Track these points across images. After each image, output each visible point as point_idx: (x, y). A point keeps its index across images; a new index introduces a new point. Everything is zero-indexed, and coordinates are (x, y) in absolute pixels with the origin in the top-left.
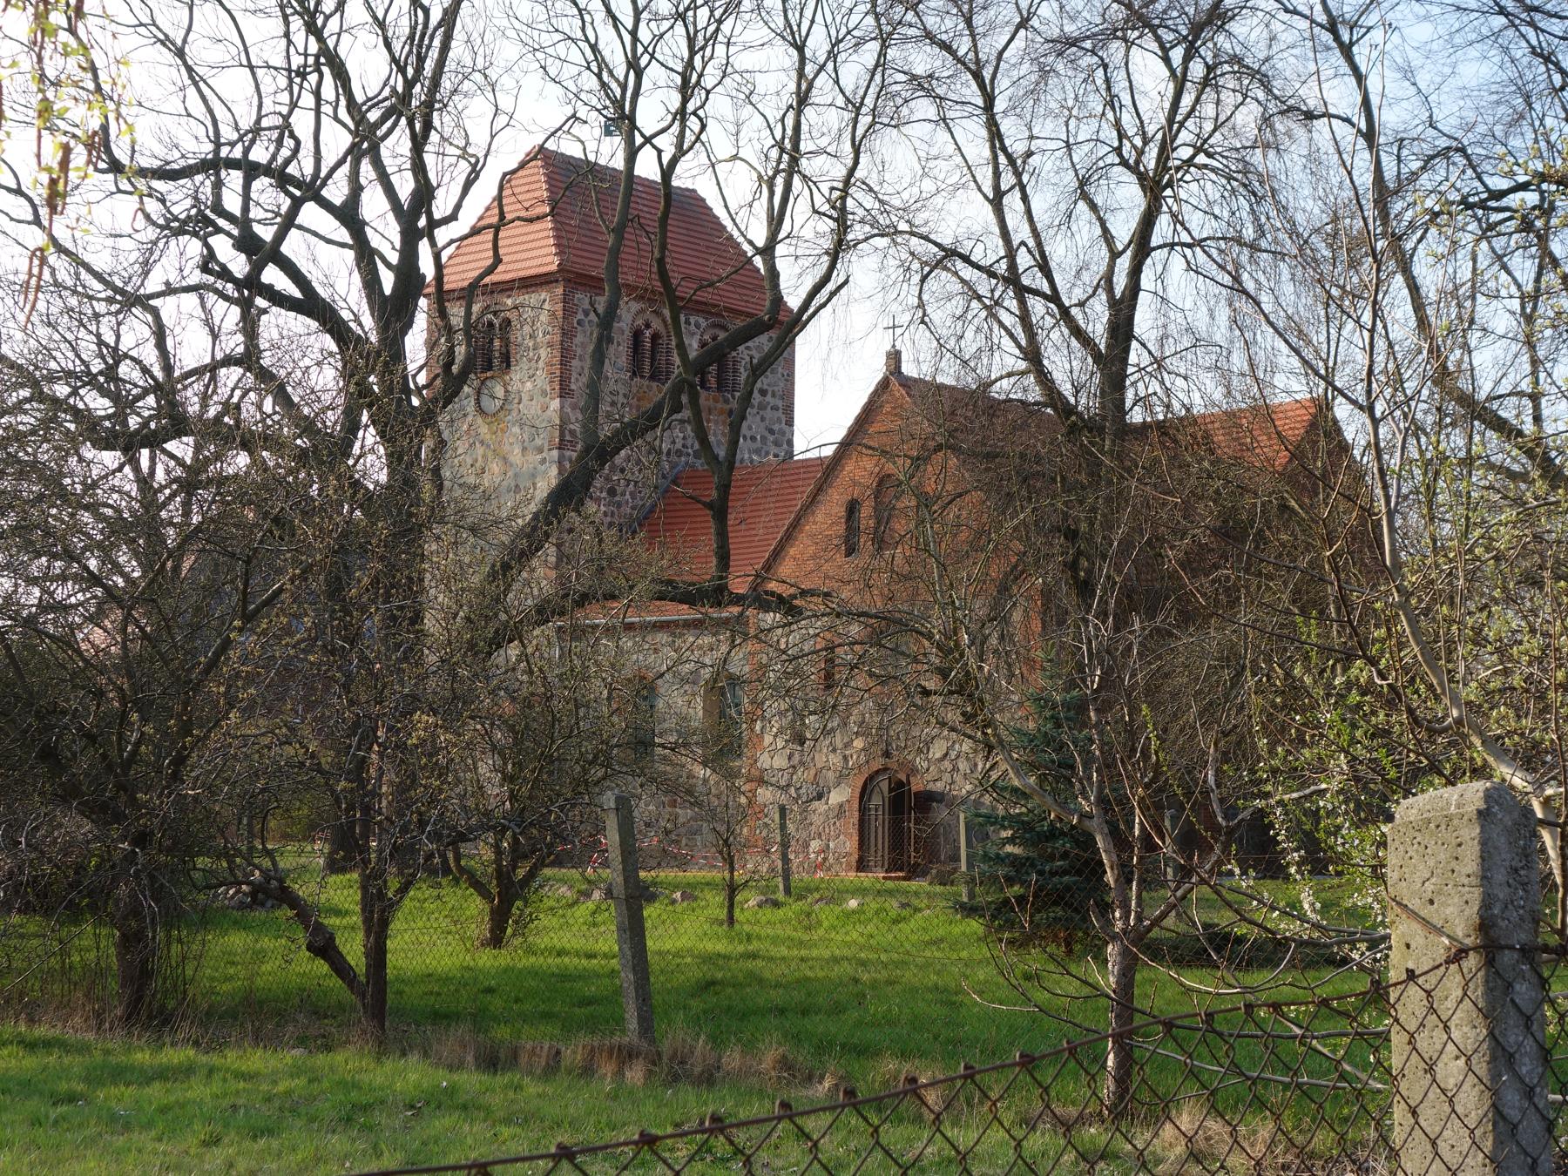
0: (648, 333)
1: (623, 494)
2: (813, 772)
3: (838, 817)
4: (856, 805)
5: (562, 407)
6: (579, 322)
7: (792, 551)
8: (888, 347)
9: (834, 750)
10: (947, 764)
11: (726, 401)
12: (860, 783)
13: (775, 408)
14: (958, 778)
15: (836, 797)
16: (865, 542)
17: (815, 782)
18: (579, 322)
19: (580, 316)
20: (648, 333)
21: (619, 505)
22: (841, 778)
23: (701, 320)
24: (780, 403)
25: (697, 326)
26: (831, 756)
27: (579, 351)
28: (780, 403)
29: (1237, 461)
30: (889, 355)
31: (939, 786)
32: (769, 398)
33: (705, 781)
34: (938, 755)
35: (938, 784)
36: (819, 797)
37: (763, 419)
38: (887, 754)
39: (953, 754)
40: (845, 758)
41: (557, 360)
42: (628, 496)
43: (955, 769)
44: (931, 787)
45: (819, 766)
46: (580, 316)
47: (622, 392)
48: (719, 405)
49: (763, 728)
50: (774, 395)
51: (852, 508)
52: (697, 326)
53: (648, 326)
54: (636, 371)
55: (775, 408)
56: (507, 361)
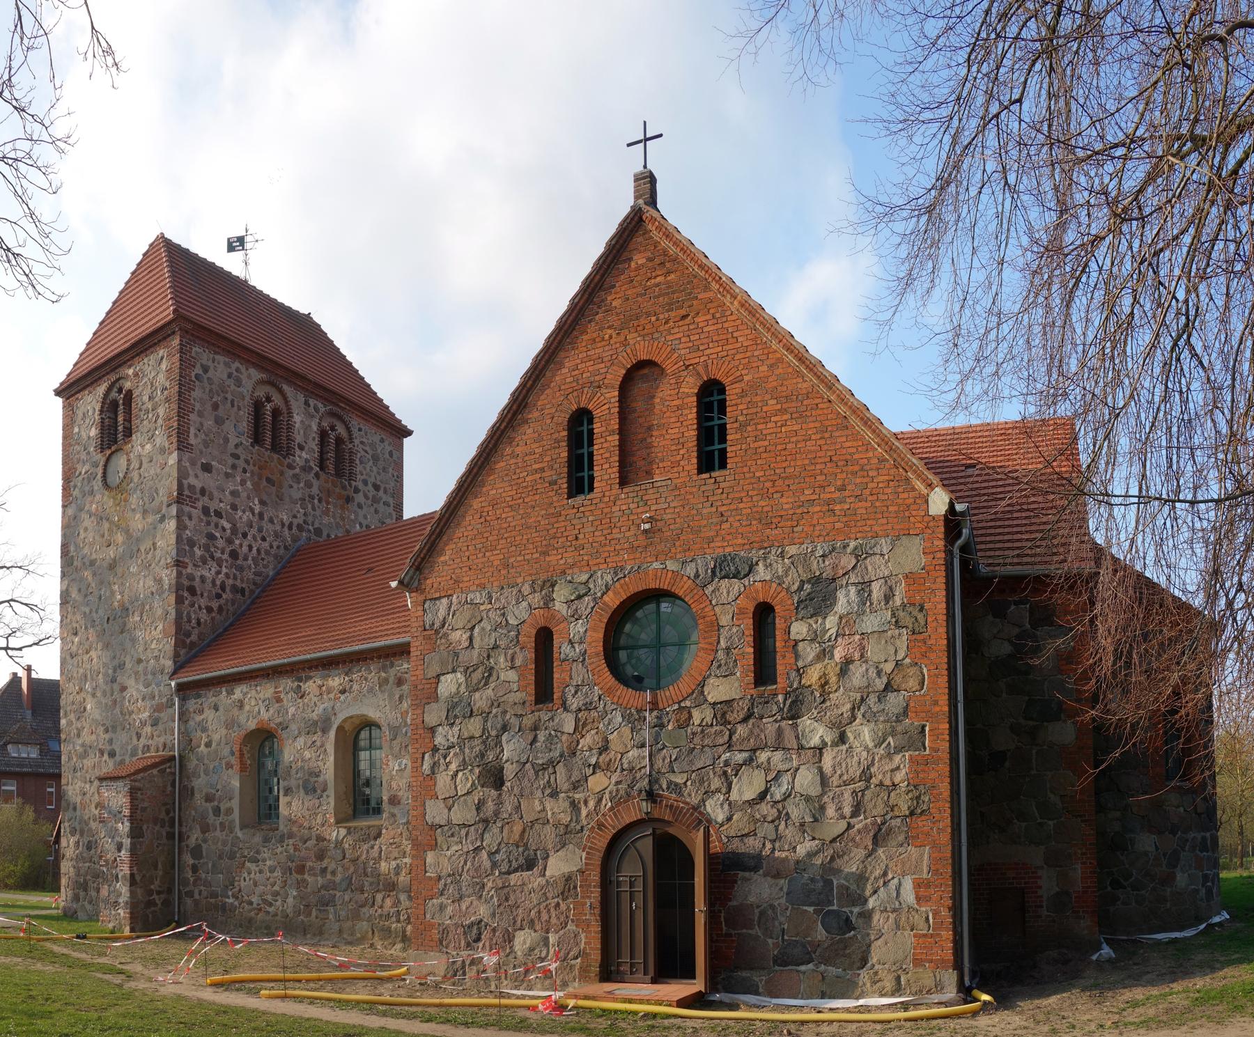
0: (268, 406)
1: (246, 559)
2: (517, 828)
3: (563, 895)
4: (595, 876)
5: (180, 461)
6: (197, 376)
7: (476, 504)
8: (640, 168)
9: (554, 794)
10: (765, 809)
11: (344, 488)
12: (602, 843)
13: (386, 504)
14: (789, 833)
15: (559, 865)
16: (605, 469)
17: (522, 842)
18: (197, 376)
19: (198, 370)
20: (268, 406)
21: (241, 569)
22: (566, 835)
23: (320, 405)
24: (391, 501)
25: (316, 409)
26: (549, 804)
27: (198, 406)
28: (391, 501)
29: (368, 783)
30: (637, 178)
31: (752, 845)
32: (381, 493)
33: (339, 843)
34: (750, 795)
35: (750, 841)
36: (530, 865)
37: (376, 511)
38: (651, 796)
39: (778, 793)
40: (574, 805)
41: (174, 413)
42: (250, 561)
43: (782, 815)
44: (736, 846)
45: (527, 818)
46: (198, 370)
47: (243, 457)
48: (337, 490)
49: (435, 765)
50: (385, 492)
51: (580, 423)
52: (316, 409)
53: (269, 399)
54: (257, 439)
55: (386, 504)
56: (128, 433)
